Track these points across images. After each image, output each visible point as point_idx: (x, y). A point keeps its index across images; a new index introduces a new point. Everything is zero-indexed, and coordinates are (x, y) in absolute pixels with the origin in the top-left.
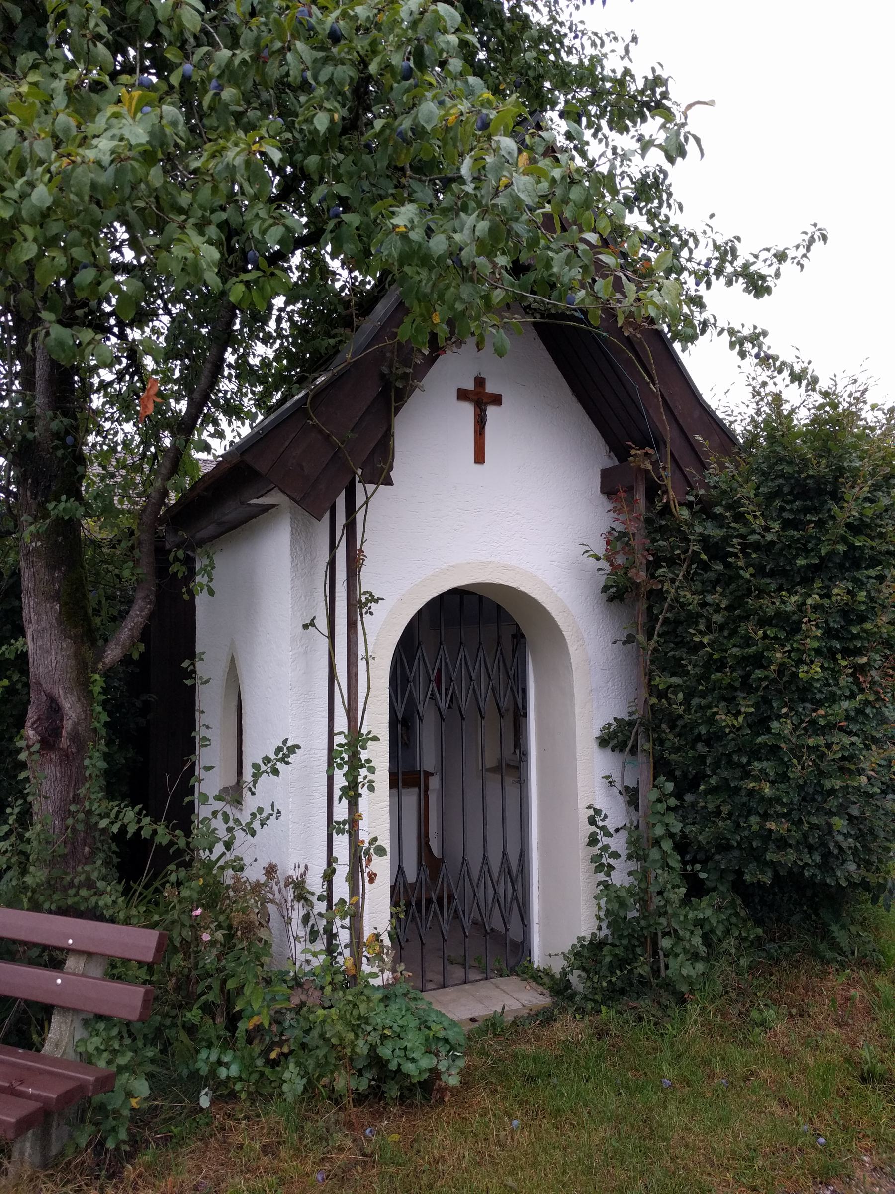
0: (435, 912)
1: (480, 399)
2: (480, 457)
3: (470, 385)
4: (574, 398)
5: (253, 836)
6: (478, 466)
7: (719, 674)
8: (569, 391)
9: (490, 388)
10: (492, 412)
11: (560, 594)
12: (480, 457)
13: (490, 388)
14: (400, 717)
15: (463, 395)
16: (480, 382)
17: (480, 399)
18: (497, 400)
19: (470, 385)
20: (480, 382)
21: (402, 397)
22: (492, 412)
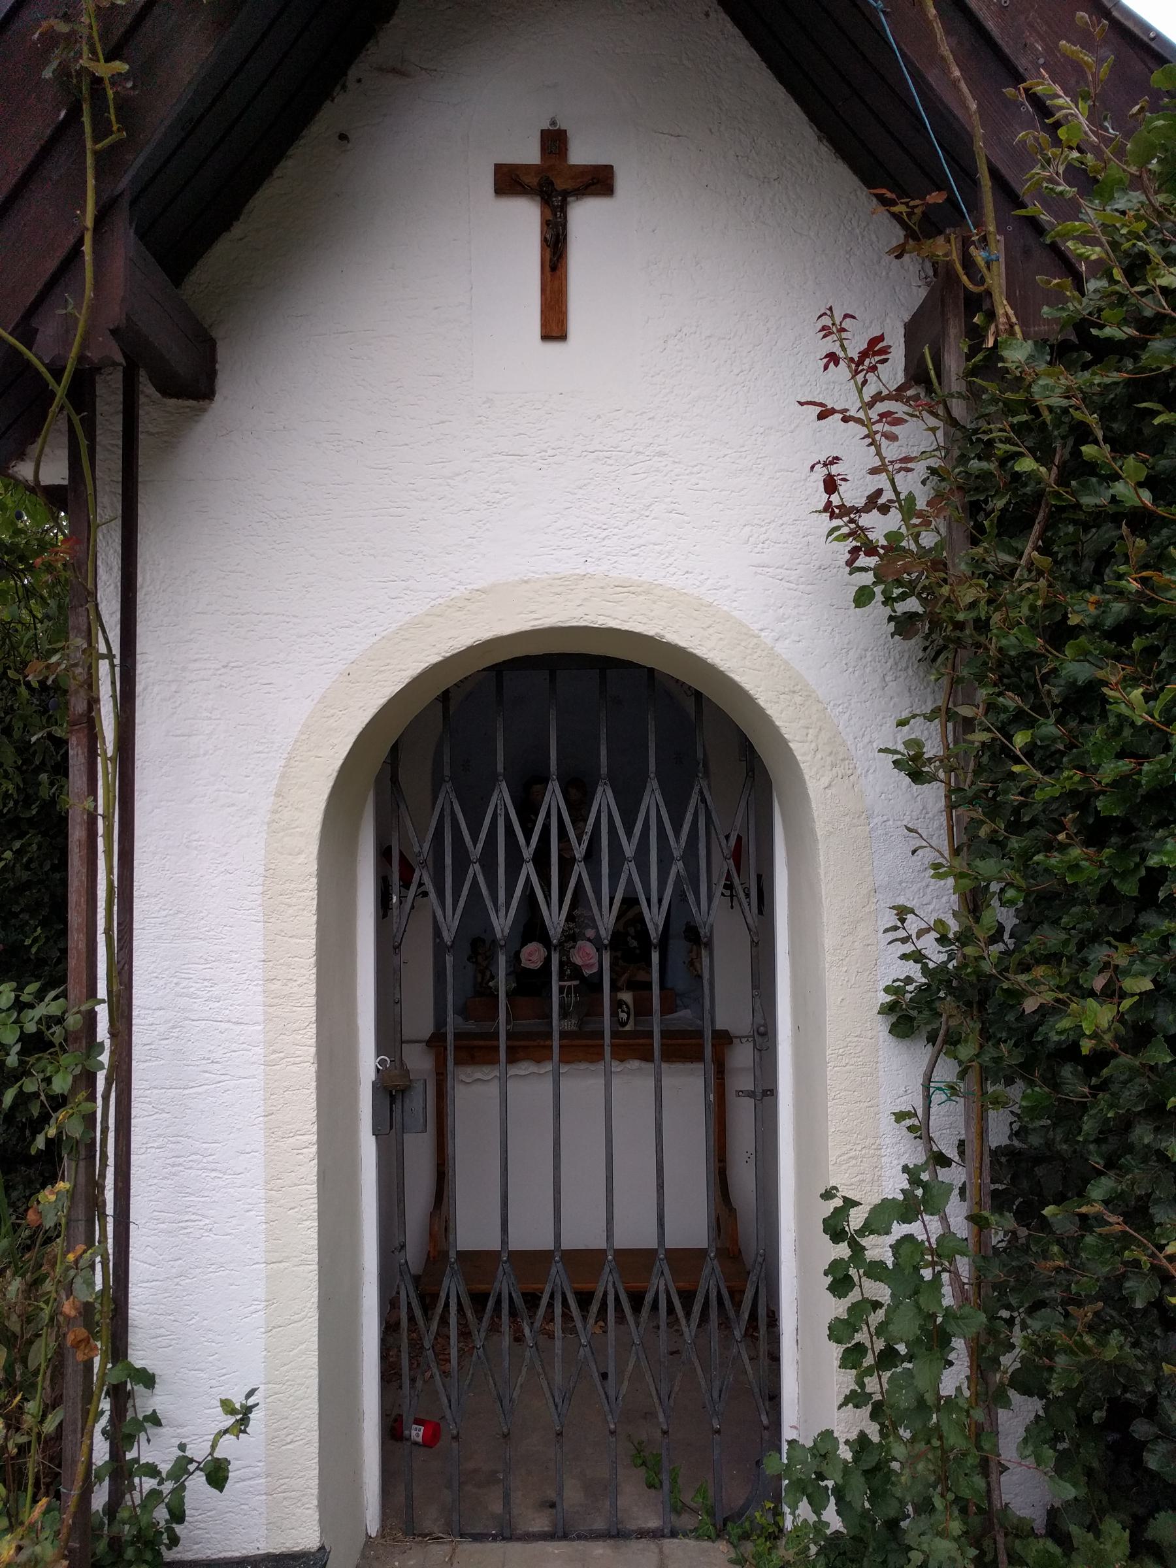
0: (738, 1305)
1: (554, 184)
2: (554, 327)
3: (530, 154)
4: (825, 150)
5: (822, 1196)
6: (554, 347)
7: (1163, 756)
8: (808, 132)
9: (581, 154)
10: (583, 215)
11: (782, 648)
12: (554, 327)
13: (581, 154)
14: (448, 937)
15: (509, 181)
16: (554, 141)
17: (554, 184)
18: (599, 181)
19: (530, 154)
20: (554, 141)
21: (932, 656)
22: (583, 215)
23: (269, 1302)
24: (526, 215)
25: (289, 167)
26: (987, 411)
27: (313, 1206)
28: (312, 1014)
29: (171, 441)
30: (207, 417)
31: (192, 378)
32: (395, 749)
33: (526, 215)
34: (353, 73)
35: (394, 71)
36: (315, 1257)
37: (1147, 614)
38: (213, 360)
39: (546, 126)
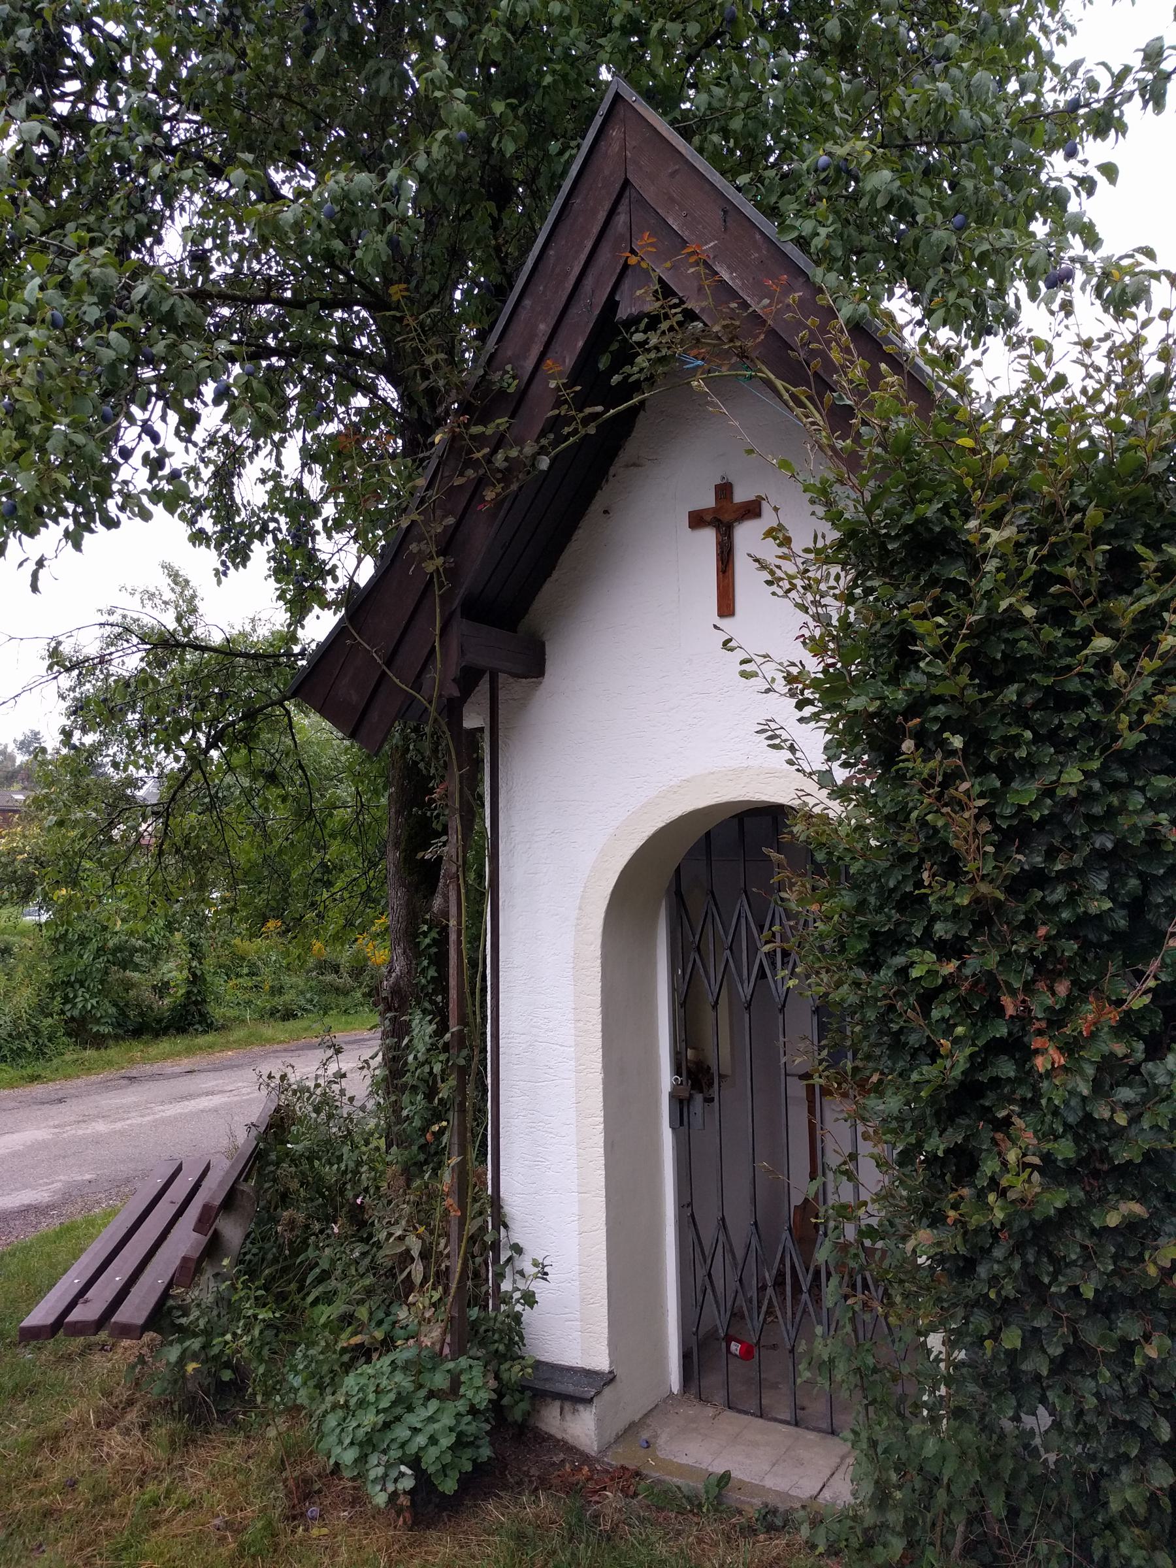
3: (708, 501)
9: (741, 496)
13: (741, 496)
15: (697, 520)
16: (724, 490)
19: (708, 501)
20: (724, 490)
23: (580, 1217)
24: (708, 538)
25: (579, 534)
26: (718, 269)
27: (602, 1161)
28: (599, 1042)
29: (523, 703)
30: (542, 687)
31: (533, 663)
32: (678, 870)
33: (708, 538)
34: (612, 471)
35: (634, 465)
36: (603, 1193)
37: (1125, 1197)
38: (544, 654)
39: (719, 482)
